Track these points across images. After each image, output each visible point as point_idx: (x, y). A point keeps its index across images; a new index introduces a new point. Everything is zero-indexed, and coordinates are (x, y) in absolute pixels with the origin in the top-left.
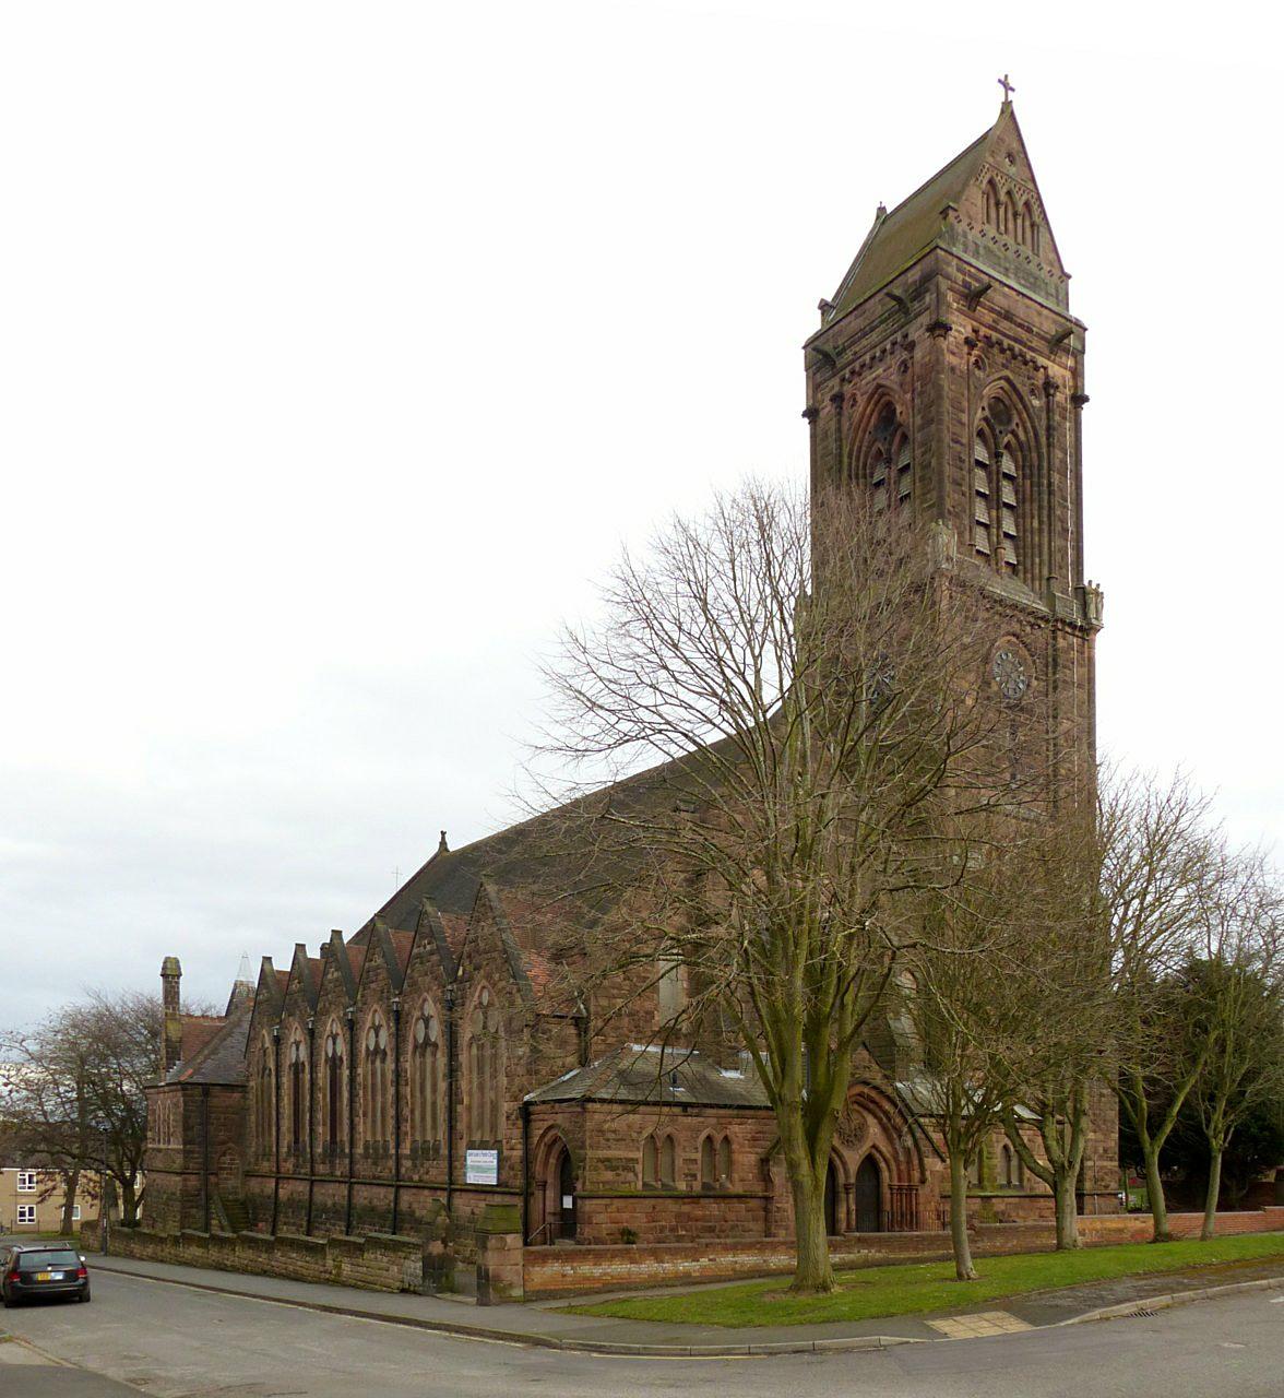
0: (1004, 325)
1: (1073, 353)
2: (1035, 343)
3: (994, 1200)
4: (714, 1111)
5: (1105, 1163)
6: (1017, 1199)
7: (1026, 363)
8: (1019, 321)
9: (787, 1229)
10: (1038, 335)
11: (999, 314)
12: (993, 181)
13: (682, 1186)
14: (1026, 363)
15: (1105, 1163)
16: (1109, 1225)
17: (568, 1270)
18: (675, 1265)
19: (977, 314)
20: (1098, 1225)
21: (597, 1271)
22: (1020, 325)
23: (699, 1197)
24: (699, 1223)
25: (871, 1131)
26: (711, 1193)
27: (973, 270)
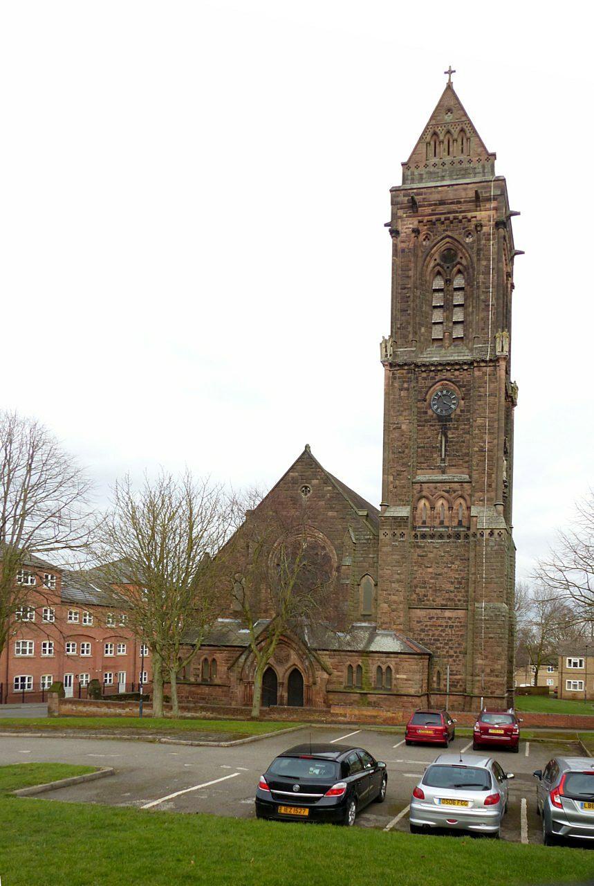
0: (441, 209)
1: (494, 198)
2: (464, 207)
3: (369, 695)
4: (207, 648)
5: (492, 679)
6: (386, 696)
7: (460, 221)
8: (450, 201)
9: (236, 701)
10: (465, 202)
11: (435, 204)
12: (449, 129)
13: (192, 680)
14: (460, 221)
15: (492, 679)
16: (365, 713)
17: (74, 708)
18: (116, 710)
19: (419, 213)
20: (357, 712)
21: (85, 709)
22: (452, 203)
23: (200, 684)
24: (199, 696)
25: (292, 657)
26: (207, 683)
27: (415, 191)
